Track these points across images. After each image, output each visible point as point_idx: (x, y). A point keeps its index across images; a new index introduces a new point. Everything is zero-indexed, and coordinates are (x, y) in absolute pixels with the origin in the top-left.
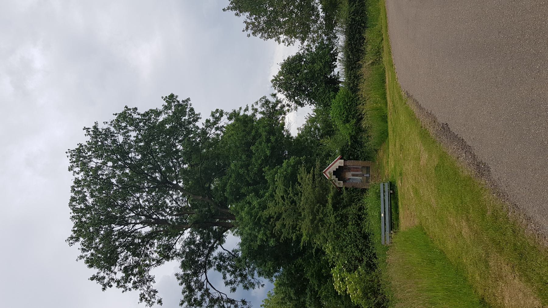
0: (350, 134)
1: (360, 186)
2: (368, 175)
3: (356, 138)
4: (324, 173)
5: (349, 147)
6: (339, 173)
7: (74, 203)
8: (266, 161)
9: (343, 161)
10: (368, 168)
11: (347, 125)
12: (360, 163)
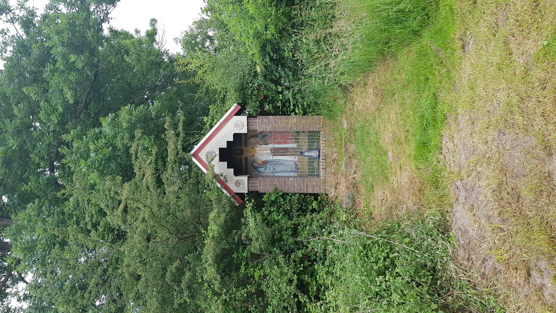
0: (258, 35)
1: (296, 186)
2: (314, 154)
3: (277, 50)
4: (195, 155)
5: (260, 78)
6: (235, 154)
7: (268, 44)
8: (71, 114)
9: (243, 119)
10: (314, 136)
12: (292, 122)
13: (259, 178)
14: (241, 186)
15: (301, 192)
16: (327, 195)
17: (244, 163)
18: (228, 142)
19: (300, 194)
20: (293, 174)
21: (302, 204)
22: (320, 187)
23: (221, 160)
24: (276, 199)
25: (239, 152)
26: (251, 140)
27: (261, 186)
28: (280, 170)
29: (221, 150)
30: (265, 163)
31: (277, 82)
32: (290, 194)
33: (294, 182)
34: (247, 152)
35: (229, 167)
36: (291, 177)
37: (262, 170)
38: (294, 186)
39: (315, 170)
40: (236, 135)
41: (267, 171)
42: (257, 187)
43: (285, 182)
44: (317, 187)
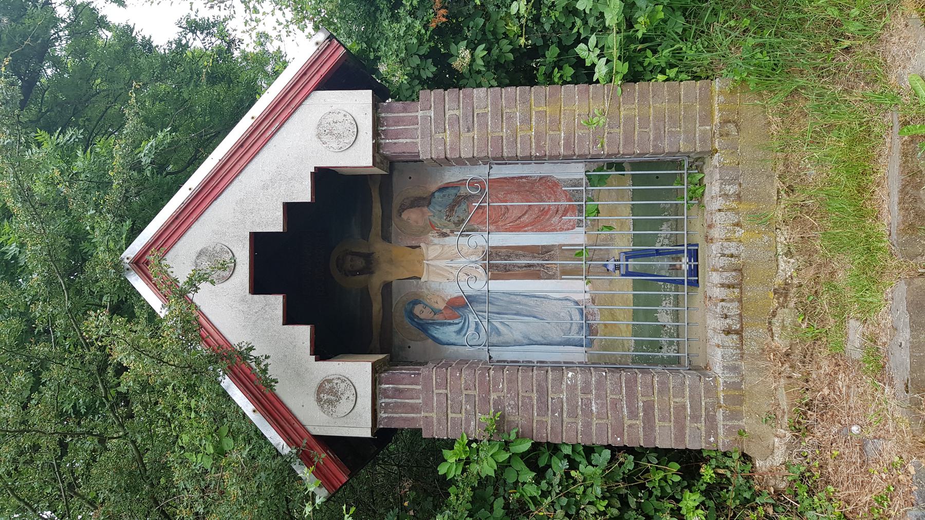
1: (594, 413)
6: (326, 261)
13: (424, 370)
14: (344, 406)
15: (618, 441)
16: (746, 458)
17: (377, 307)
18: (290, 209)
19: (615, 450)
20: (578, 354)
21: (624, 500)
22: (711, 421)
23: (258, 286)
24: (502, 467)
25: (360, 263)
26: (405, 216)
27: (438, 406)
28: (518, 336)
29: (258, 241)
30: (459, 306)
32: (567, 450)
33: (586, 390)
34: (391, 261)
35: (290, 318)
36: (570, 365)
37: (447, 333)
38: (587, 412)
39: (664, 339)
40: (323, 178)
41: (464, 338)
42: (414, 409)
43: (543, 392)
44: (695, 418)
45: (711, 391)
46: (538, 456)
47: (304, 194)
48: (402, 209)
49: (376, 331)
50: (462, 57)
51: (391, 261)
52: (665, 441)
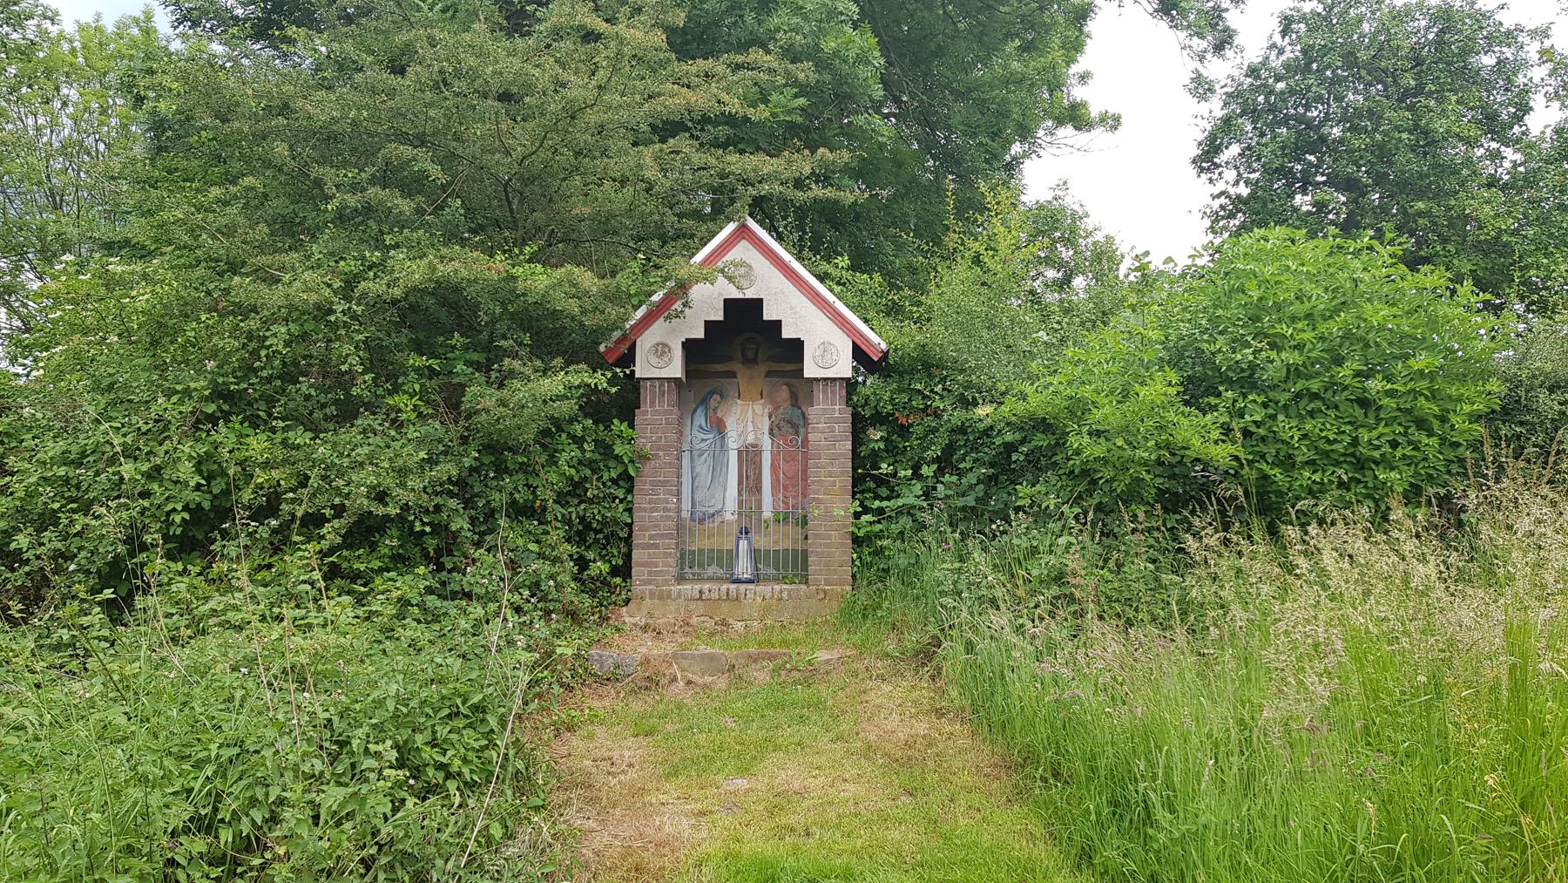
0: (1078, 409)
1: (651, 516)
2: (743, 568)
3: (1037, 464)
4: (743, 232)
5: (957, 416)
6: (745, 343)
9: (844, 366)
10: (795, 565)
11: (1160, 387)
12: (835, 506)
13: (675, 410)
14: (654, 360)
15: (635, 528)
16: (627, 602)
17: (719, 367)
18: (777, 325)
19: (630, 526)
21: (600, 531)
22: (649, 582)
24: (618, 458)
25: (750, 354)
27: (654, 415)
28: (698, 469)
29: (758, 303)
30: (719, 428)
31: (945, 463)
33: (665, 509)
34: (751, 378)
37: (700, 419)
38: (652, 510)
40: (798, 345)
41: (697, 434)
42: (652, 404)
43: (664, 483)
45: (666, 582)
46: (627, 481)
47: (787, 333)
48: (789, 385)
49: (701, 367)
50: (876, 434)
51: (751, 378)
52: (637, 555)
